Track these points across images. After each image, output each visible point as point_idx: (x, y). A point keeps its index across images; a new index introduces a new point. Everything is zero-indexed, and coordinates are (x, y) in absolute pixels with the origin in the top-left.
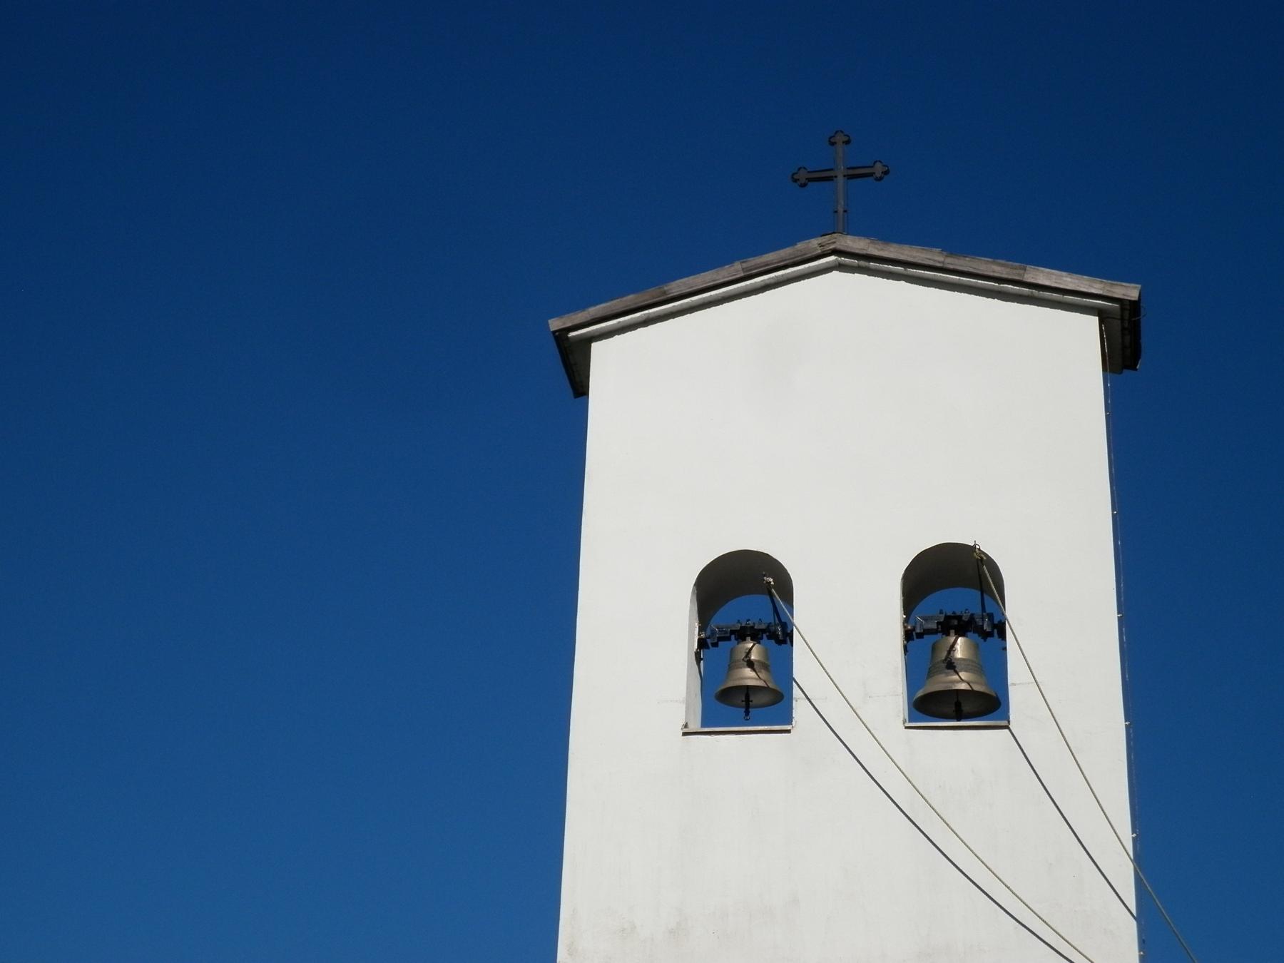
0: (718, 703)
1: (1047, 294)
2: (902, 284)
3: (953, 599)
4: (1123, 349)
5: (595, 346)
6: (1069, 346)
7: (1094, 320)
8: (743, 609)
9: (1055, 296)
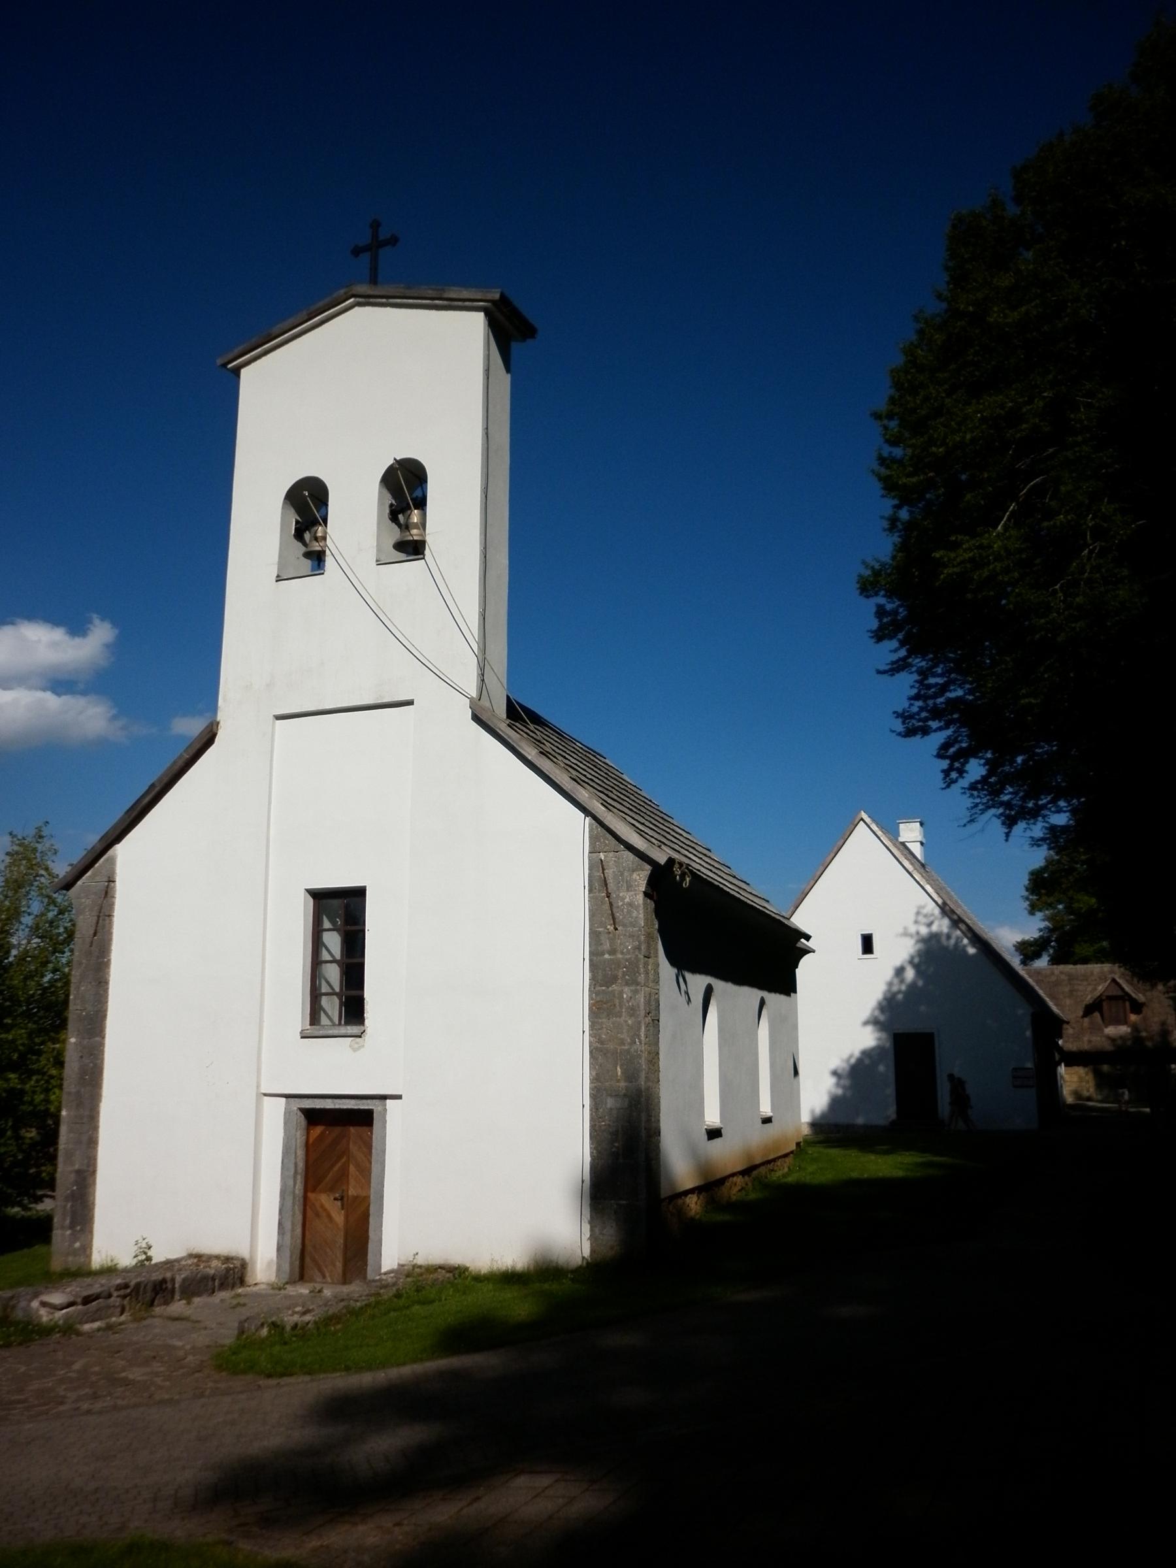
0: (1025, 880)
1: (467, 304)
2: (388, 309)
3: (406, 486)
4: (508, 330)
5: (243, 372)
6: (468, 330)
7: (482, 314)
8: (308, 503)
9: (460, 303)
